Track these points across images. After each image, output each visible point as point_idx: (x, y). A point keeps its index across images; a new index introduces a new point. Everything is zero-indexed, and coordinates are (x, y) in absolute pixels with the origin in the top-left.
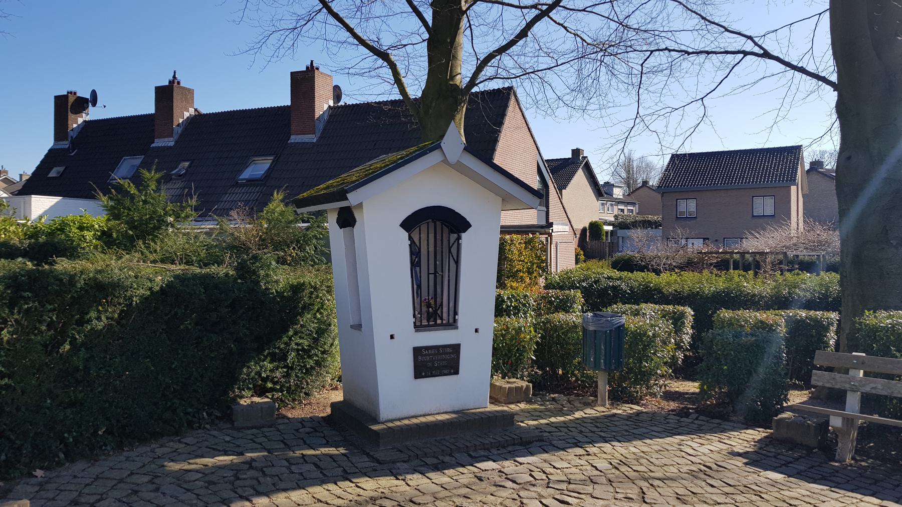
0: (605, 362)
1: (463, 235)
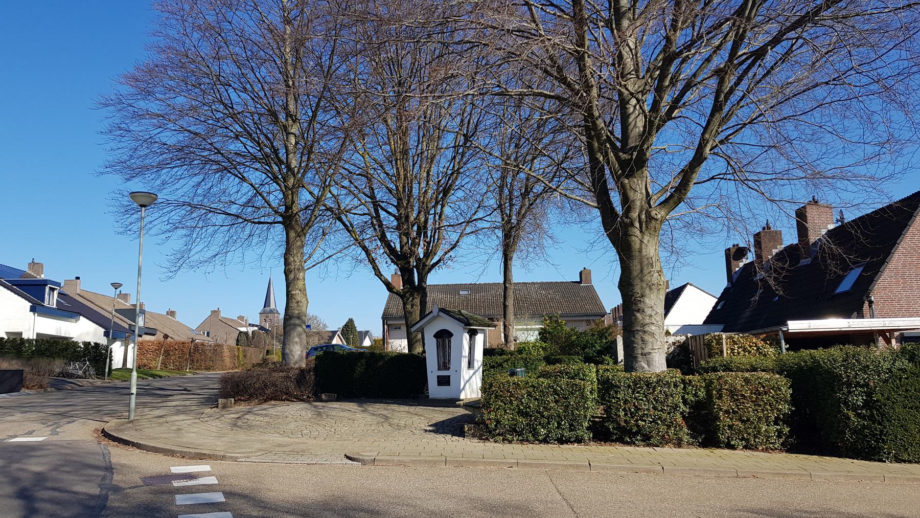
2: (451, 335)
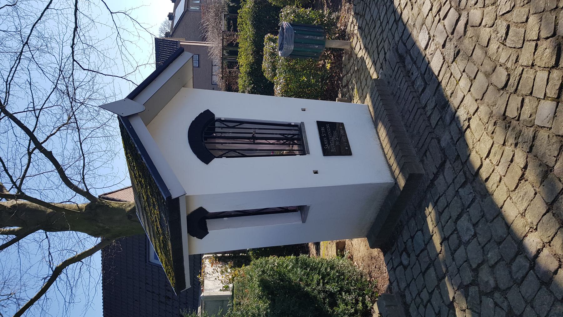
0: (319, 36)
1: (217, 116)
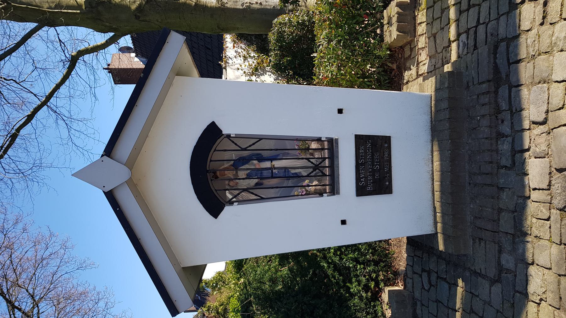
1: (225, 132)
2: (212, 133)
